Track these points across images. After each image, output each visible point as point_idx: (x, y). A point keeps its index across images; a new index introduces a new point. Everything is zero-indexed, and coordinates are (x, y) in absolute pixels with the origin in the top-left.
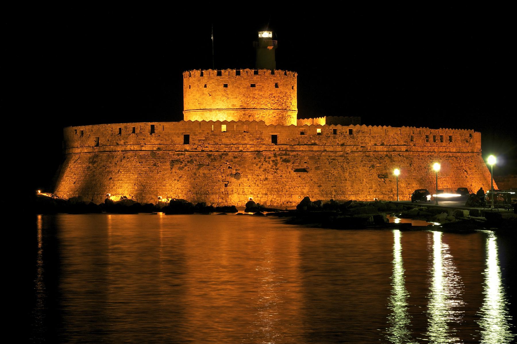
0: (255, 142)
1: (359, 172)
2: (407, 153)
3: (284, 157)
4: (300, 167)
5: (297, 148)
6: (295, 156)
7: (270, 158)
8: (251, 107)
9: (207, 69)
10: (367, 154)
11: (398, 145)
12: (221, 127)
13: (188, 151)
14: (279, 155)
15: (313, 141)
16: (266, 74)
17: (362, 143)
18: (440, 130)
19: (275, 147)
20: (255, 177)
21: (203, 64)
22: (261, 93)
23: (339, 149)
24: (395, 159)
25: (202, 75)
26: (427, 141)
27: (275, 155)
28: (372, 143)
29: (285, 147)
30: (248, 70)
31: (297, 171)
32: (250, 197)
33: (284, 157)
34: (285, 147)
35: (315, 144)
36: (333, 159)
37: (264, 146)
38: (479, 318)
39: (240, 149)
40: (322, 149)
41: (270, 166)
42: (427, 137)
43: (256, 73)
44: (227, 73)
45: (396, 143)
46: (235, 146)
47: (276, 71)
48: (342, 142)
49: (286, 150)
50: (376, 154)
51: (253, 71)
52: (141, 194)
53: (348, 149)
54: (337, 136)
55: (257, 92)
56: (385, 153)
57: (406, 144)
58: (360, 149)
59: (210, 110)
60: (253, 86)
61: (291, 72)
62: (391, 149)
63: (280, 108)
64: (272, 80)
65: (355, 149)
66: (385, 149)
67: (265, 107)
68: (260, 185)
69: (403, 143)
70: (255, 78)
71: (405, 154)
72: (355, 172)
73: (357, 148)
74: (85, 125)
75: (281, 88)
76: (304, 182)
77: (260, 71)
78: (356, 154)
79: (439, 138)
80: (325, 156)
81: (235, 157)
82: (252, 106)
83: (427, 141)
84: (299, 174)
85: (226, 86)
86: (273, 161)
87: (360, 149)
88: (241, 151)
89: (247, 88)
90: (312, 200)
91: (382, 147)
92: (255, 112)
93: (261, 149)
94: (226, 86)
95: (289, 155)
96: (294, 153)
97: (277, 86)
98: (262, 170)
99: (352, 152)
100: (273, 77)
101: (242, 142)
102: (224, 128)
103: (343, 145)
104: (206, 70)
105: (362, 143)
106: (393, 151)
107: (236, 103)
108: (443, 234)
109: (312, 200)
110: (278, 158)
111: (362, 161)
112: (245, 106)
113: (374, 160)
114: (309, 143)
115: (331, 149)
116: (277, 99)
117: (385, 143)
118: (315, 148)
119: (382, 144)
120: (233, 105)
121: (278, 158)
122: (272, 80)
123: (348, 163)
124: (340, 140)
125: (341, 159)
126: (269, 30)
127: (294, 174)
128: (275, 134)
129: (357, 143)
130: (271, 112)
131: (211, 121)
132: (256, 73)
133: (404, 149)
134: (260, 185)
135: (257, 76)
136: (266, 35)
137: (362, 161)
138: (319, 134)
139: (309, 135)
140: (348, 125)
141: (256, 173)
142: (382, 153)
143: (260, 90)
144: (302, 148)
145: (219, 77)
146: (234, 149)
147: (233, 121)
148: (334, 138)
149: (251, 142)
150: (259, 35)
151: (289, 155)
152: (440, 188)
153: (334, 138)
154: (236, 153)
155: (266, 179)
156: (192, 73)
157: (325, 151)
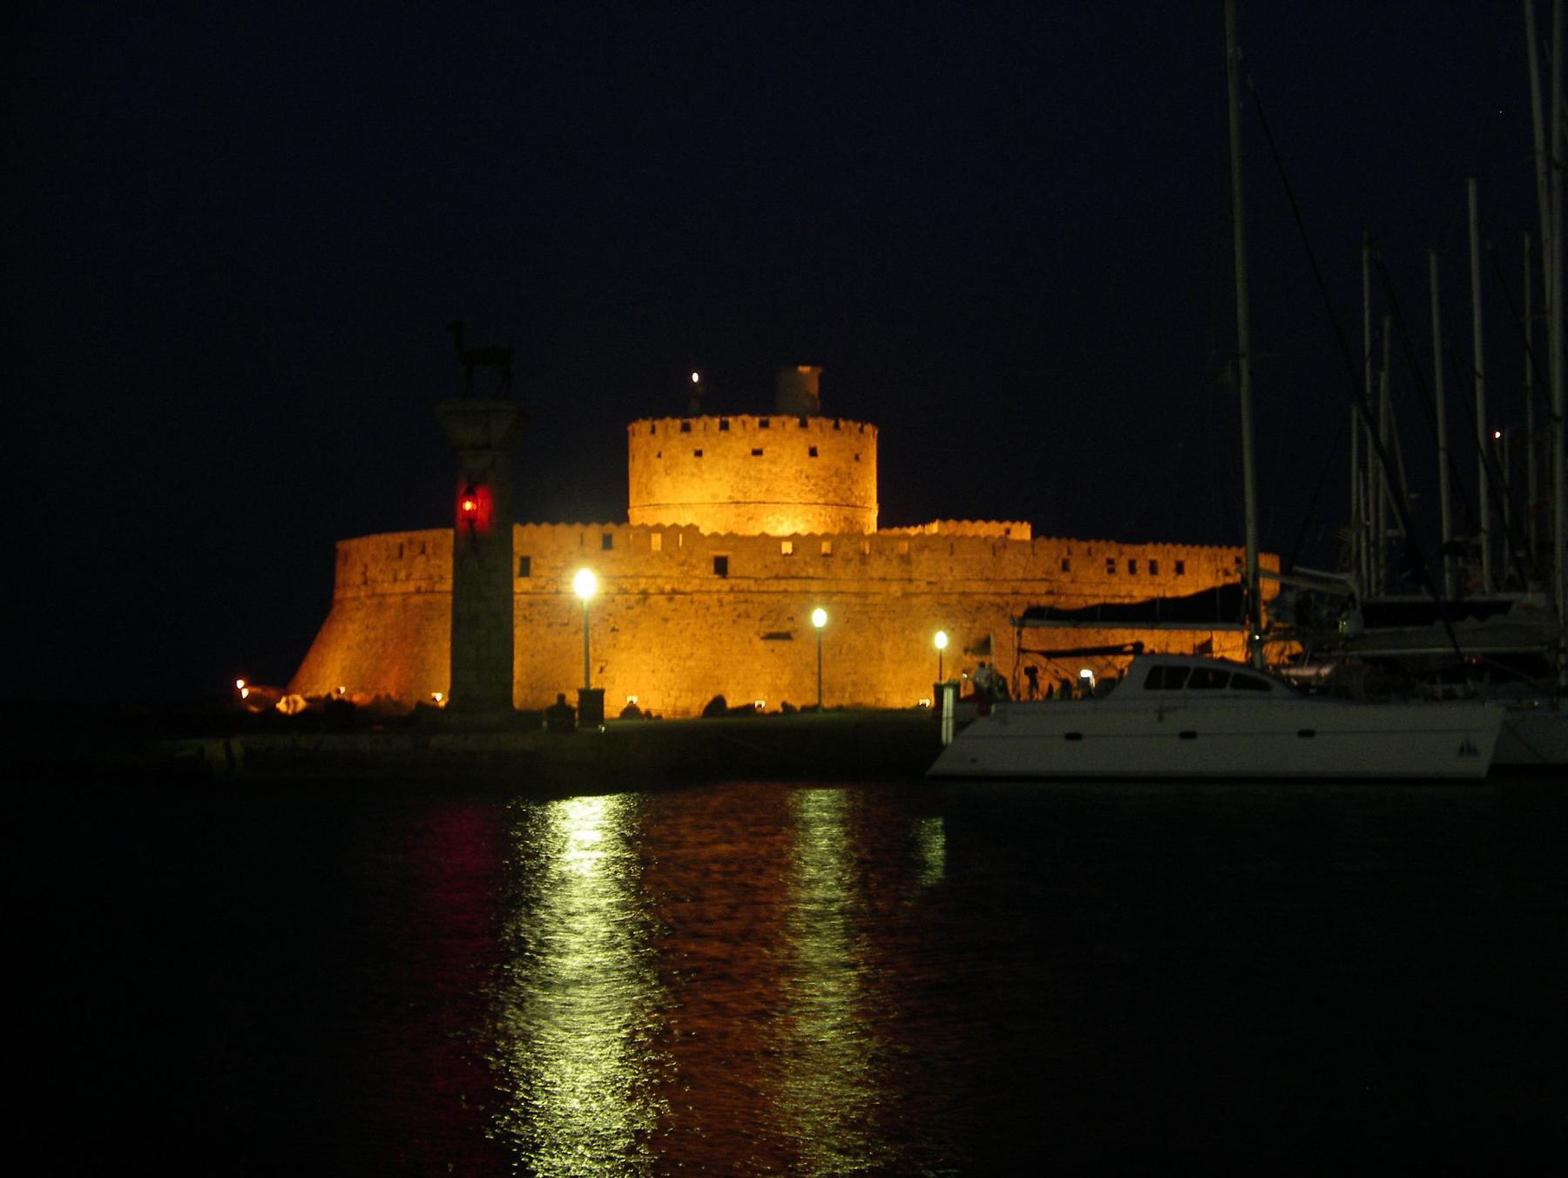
0: (675, 572)
4: (775, 630)
9: (662, 418)
11: (1025, 580)
12: (650, 539)
18: (1149, 548)
21: (680, 406)
22: (775, 469)
26: (1111, 571)
30: (745, 417)
31: (770, 637)
32: (635, 700)
34: (744, 584)
37: (696, 582)
38: (660, 1040)
42: (1110, 562)
43: (764, 425)
47: (810, 421)
51: (717, 420)
52: (1225, 675)
55: (765, 466)
59: (667, 506)
60: (757, 453)
61: (851, 423)
62: (1006, 588)
66: (992, 589)
70: (762, 436)
77: (774, 421)
79: (1146, 566)
83: (1111, 571)
84: (772, 644)
85: (699, 454)
89: (745, 458)
90: (731, 703)
94: (699, 454)
100: (802, 433)
102: (656, 540)
108: (643, 808)
109: (731, 703)
120: (713, 496)
127: (760, 645)
128: (722, 553)
131: (675, 527)
138: (826, 555)
143: (774, 462)
145: (684, 435)
147: (811, 536)
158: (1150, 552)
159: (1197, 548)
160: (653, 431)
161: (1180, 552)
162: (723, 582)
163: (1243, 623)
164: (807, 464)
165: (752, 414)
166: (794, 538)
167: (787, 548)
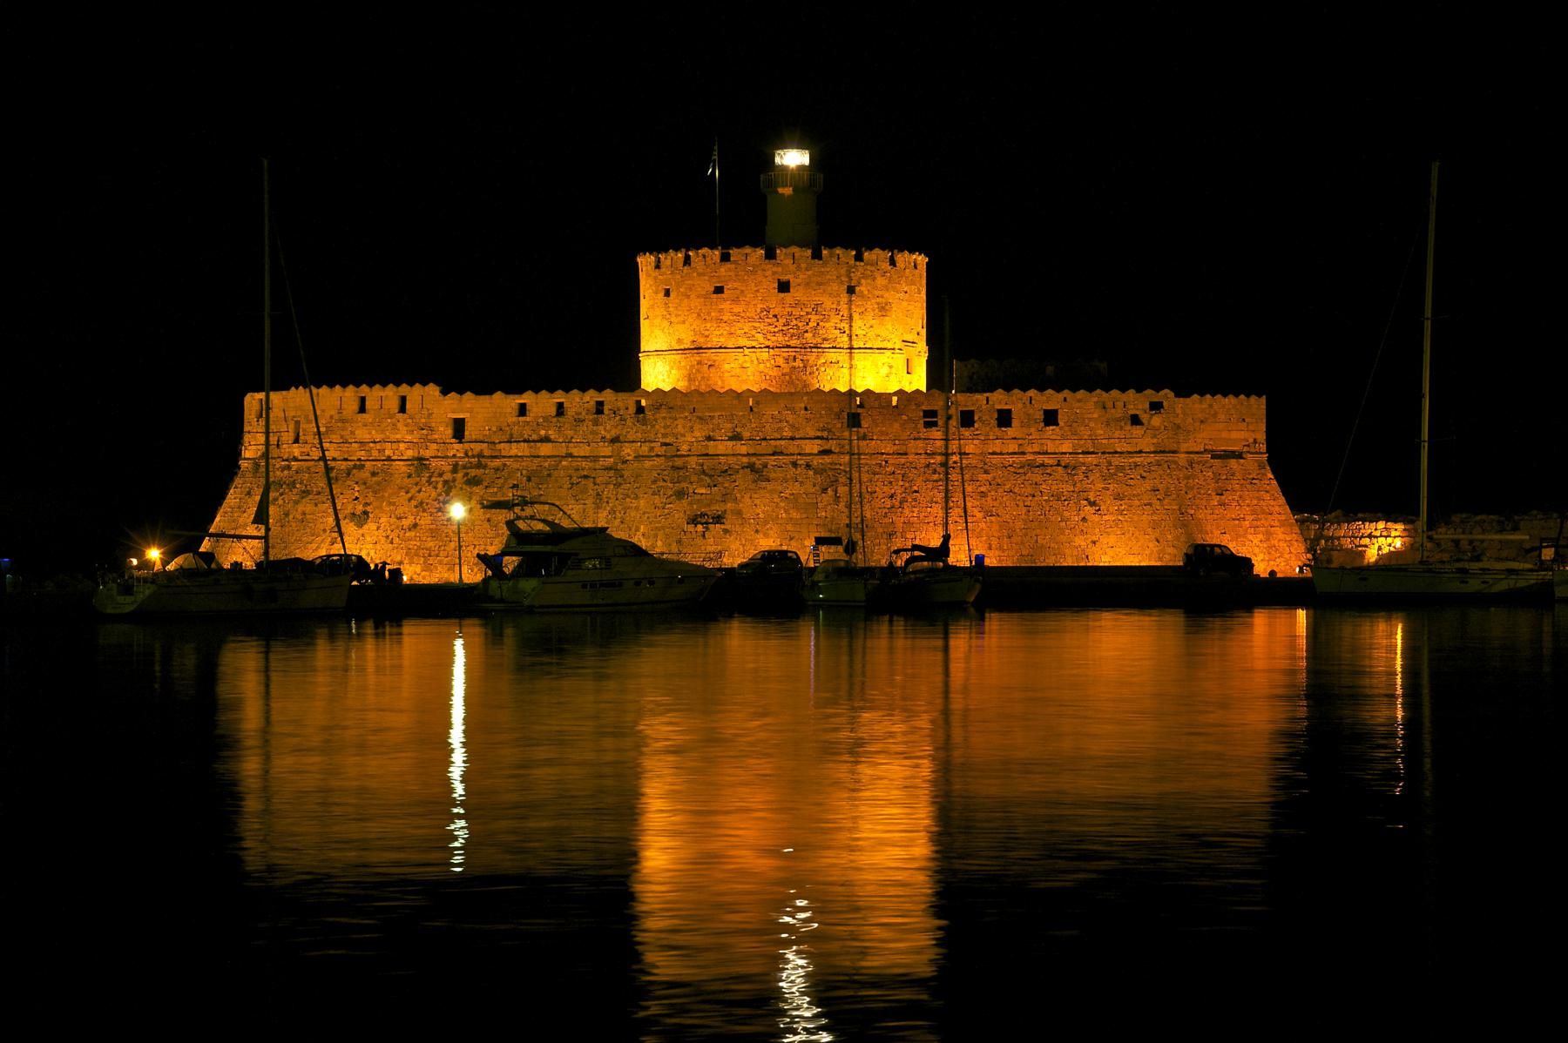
1: (637, 508)
2: (827, 459)
3: (473, 472)
5: (505, 449)
6: (497, 470)
7: (441, 475)
8: (714, 344)
9: (666, 251)
10: (679, 462)
11: (792, 439)
13: (295, 459)
14: (464, 467)
15: (543, 433)
16: (751, 260)
17: (665, 435)
19: (457, 449)
20: (393, 520)
23: (606, 450)
24: (773, 475)
25: (687, 260)
26: (928, 425)
27: (455, 470)
28: (697, 434)
29: (477, 447)
30: (705, 250)
33: (473, 472)
34: (477, 447)
35: (546, 440)
36: (585, 477)
37: (434, 446)
39: (387, 453)
40: (563, 452)
41: (434, 495)
43: (725, 258)
44: (668, 262)
45: (787, 433)
46: (378, 446)
48: (614, 433)
49: (480, 455)
50: (708, 463)
53: (628, 451)
54: (603, 418)
55: (726, 306)
56: (745, 460)
57: (825, 434)
58: (659, 450)
62: (764, 447)
63: (793, 343)
64: (769, 273)
65: (645, 449)
66: (744, 450)
67: (749, 344)
68: (396, 540)
69: (812, 434)
70: (724, 270)
71: (816, 461)
72: (626, 509)
73: (652, 449)
74: (513, 387)
75: (796, 293)
76: (492, 534)
77: (734, 252)
78: (648, 464)
80: (565, 468)
81: (374, 474)
82: (715, 341)
85: (667, 293)
86: (446, 482)
87: (659, 450)
88: (389, 459)
91: (730, 443)
92: (721, 356)
93: (427, 454)
95: (485, 467)
96: (497, 463)
97: (784, 287)
98: (414, 503)
99: (638, 457)
100: (770, 268)
101: (394, 437)
103: (615, 440)
104: (738, 247)
105: (665, 435)
106: (774, 454)
107: (683, 336)
110: (460, 475)
111: (654, 482)
112: (701, 341)
113: (695, 478)
114: (535, 437)
115: (584, 450)
116: (782, 321)
117: (746, 434)
118: (545, 449)
119: (736, 437)
120: (680, 341)
121: (460, 475)
122: (769, 273)
123: (618, 485)
124: (608, 428)
125: (602, 477)
126: (800, 146)
128: (461, 416)
129: (652, 437)
130: (765, 355)
132: (725, 258)
133: (813, 447)
134: (396, 540)
135: (728, 265)
136: (793, 158)
137: (654, 482)
139: (537, 418)
140: (519, 391)
141: (400, 511)
142: (732, 460)
143: (736, 301)
144: (515, 449)
146: (375, 454)
148: (596, 423)
149: (409, 438)
150: (778, 160)
151: (485, 467)
152: (935, 542)
153: (596, 423)
154: (379, 464)
155: (415, 525)
156: (904, 258)
157: (571, 455)
158: (1014, 401)
159: (1082, 393)
160: (658, 267)
161: (1051, 399)
162: (457, 446)
163: (470, 499)
164: (775, 301)
165: (846, 247)
166: (900, 393)
167: (895, 399)
